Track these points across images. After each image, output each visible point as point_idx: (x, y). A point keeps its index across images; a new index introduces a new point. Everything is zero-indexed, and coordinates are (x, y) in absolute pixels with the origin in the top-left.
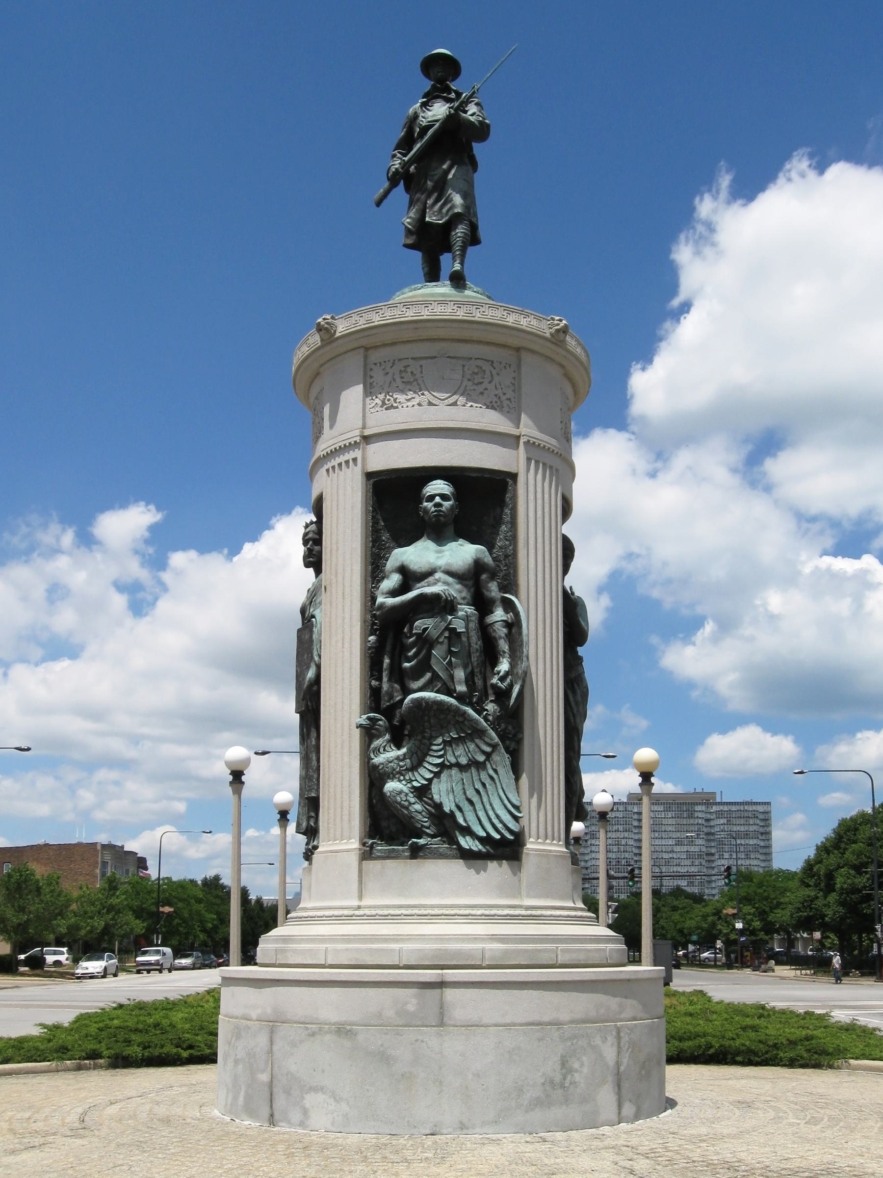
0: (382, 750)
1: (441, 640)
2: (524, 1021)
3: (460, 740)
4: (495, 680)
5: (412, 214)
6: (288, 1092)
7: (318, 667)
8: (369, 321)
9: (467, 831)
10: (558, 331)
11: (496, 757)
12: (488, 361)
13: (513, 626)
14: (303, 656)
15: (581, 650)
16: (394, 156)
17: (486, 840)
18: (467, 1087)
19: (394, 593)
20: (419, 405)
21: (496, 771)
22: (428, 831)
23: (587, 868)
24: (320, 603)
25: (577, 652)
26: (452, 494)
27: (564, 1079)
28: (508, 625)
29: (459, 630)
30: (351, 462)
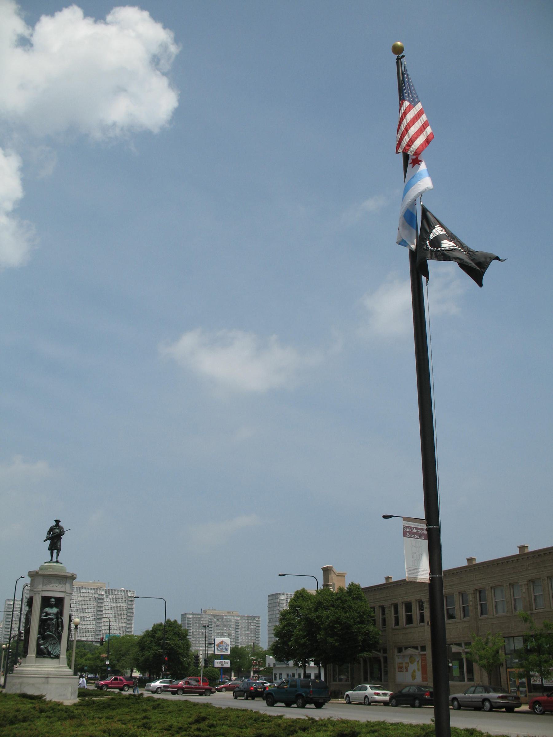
13: (62, 622)
23: (100, 631)
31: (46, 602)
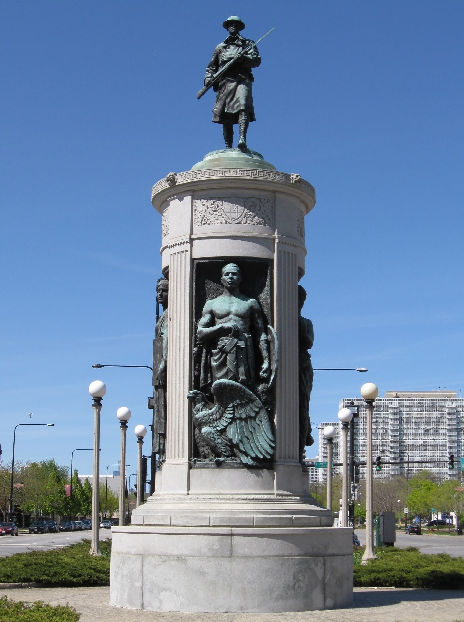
0: (200, 410)
1: (232, 352)
3: (242, 406)
5: (217, 106)
7: (166, 362)
12: (258, 199)
14: (157, 355)
17: (255, 459)
18: (244, 589)
19: (208, 325)
20: (221, 223)
21: (261, 421)
22: (225, 453)
24: (167, 326)
25: (307, 352)
26: (238, 271)
27: (295, 584)
29: (241, 347)
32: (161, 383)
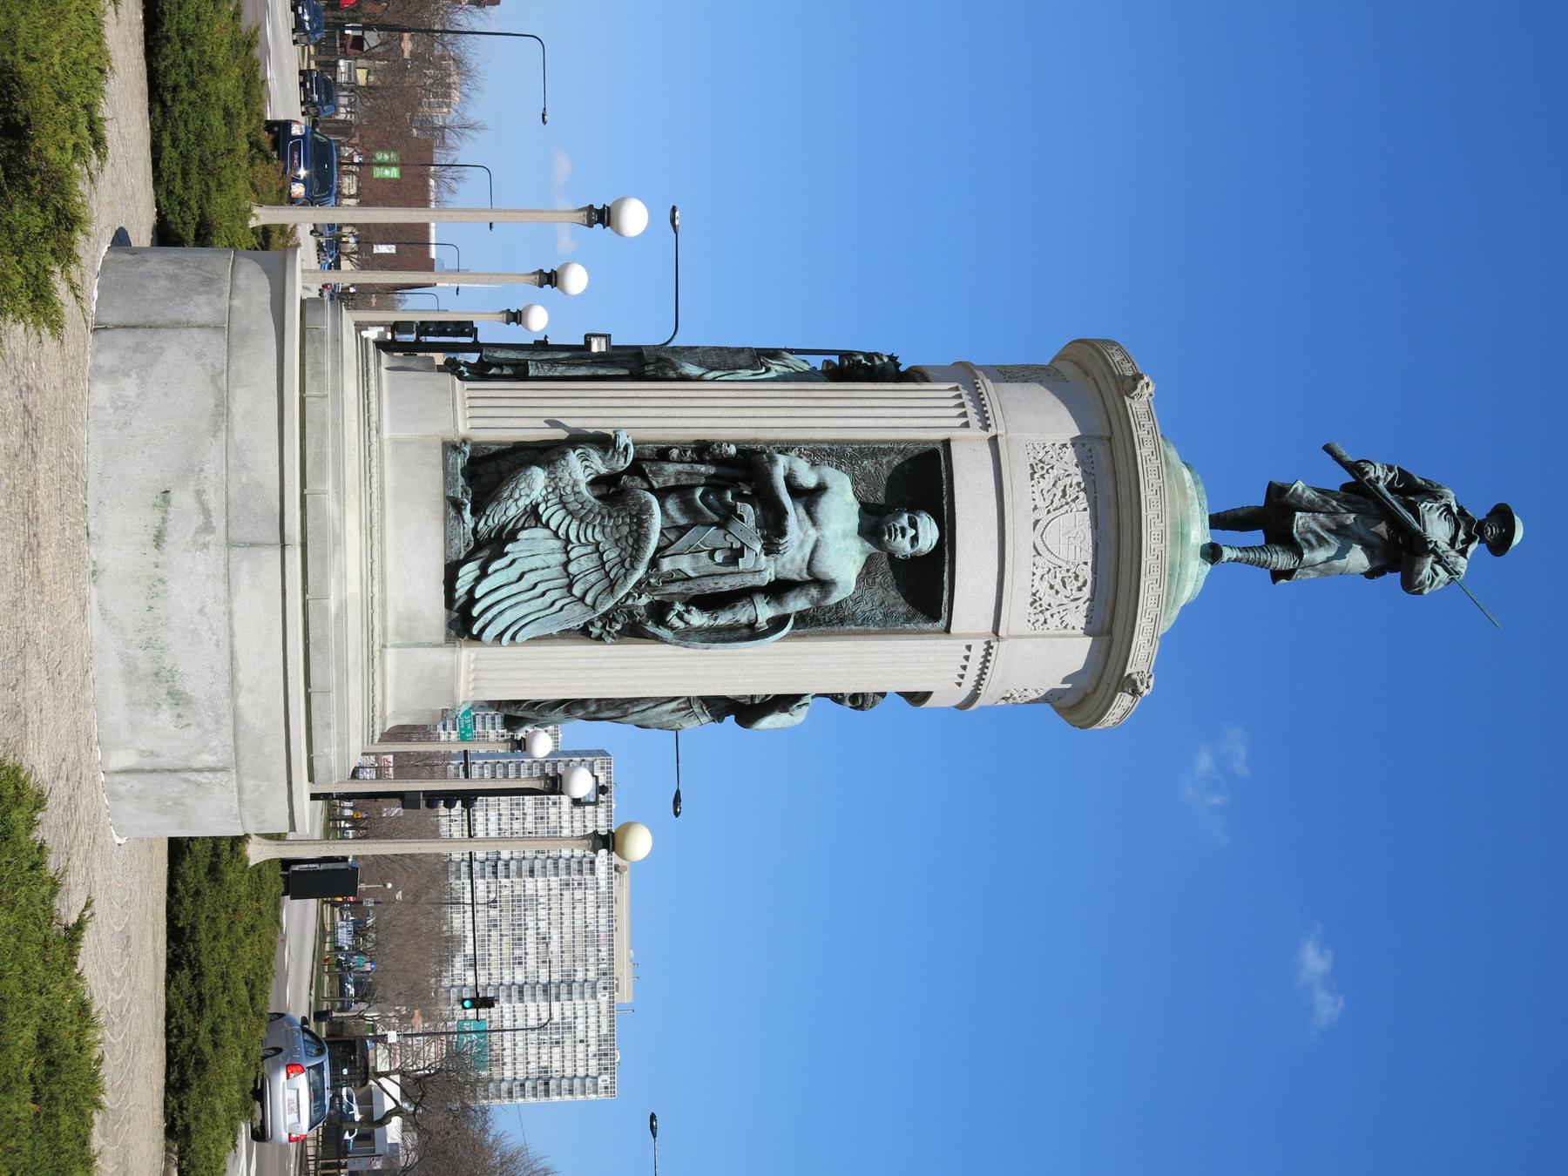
2: (237, 645)
4: (679, 607)
6: (137, 349)
7: (699, 379)
8: (1142, 442)
9: (483, 574)
10: (1134, 682)
11: (579, 608)
13: (752, 632)
15: (730, 720)
16: (1391, 469)
17: (471, 600)
19: (790, 479)
28: (751, 625)
30: (964, 420)
31: (919, 480)
32: (640, 365)
